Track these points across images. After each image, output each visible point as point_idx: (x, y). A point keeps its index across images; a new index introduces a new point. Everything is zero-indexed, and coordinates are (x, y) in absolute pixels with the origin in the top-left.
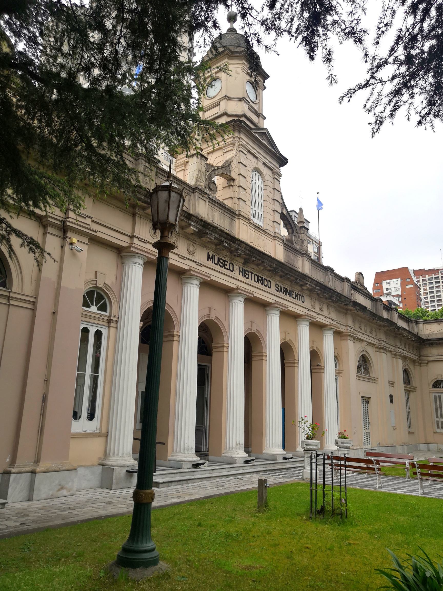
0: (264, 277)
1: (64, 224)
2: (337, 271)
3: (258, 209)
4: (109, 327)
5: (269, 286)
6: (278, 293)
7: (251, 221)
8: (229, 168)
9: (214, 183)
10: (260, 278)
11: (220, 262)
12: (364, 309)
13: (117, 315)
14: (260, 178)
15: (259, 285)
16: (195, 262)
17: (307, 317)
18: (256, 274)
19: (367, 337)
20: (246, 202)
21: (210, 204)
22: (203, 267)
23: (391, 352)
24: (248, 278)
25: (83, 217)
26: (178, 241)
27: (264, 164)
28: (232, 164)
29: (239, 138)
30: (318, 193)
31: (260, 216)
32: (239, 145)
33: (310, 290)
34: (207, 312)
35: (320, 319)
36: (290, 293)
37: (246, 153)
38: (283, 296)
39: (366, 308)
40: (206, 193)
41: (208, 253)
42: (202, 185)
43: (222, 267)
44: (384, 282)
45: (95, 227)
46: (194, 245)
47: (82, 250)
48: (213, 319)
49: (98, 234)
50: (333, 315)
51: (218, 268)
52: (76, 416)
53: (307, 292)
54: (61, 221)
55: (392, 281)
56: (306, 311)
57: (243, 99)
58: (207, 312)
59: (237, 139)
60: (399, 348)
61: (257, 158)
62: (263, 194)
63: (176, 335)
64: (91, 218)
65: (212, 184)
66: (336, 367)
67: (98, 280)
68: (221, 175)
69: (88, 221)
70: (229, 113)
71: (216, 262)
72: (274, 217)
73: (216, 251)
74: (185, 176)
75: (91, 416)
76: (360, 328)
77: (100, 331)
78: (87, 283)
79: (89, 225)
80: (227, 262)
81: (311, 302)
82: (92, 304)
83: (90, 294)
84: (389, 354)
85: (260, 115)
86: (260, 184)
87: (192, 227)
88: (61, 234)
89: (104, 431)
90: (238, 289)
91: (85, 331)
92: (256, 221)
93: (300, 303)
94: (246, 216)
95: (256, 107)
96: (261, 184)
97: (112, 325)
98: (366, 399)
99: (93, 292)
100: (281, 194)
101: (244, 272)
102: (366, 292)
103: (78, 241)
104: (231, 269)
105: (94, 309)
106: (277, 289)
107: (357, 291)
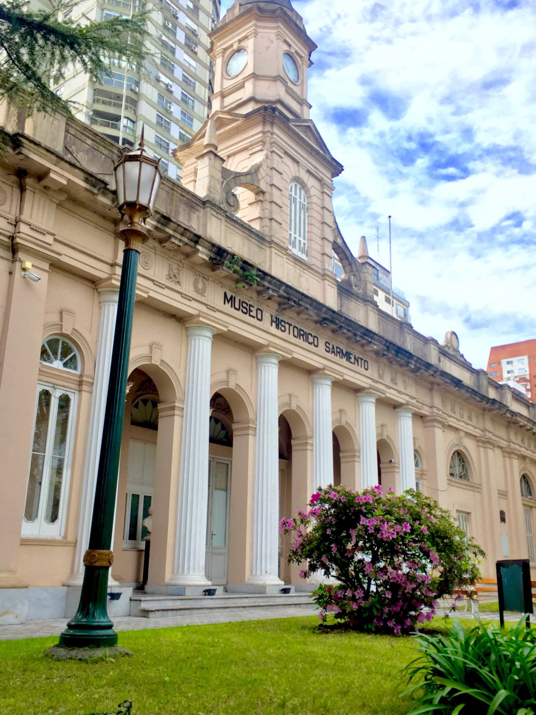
1: (12, 241)
2: (415, 328)
3: (296, 232)
4: (80, 391)
5: (316, 344)
7: (288, 252)
8: (257, 175)
9: (234, 195)
10: (302, 333)
11: (243, 307)
12: (458, 383)
13: (91, 373)
14: (303, 192)
15: (300, 342)
16: (206, 305)
17: (371, 391)
18: (297, 325)
19: (463, 424)
20: (281, 224)
21: (228, 225)
23: (501, 448)
24: (284, 331)
25: (41, 232)
26: (181, 273)
28: (261, 170)
30: (390, 217)
31: (302, 245)
32: (271, 144)
33: (377, 353)
34: (223, 376)
35: (392, 395)
36: (348, 356)
37: (282, 155)
38: (337, 359)
39: (460, 381)
40: (221, 209)
41: (225, 293)
42: (218, 197)
43: (246, 313)
44: (504, 362)
45: (58, 247)
46: (204, 280)
47: (39, 279)
48: (233, 388)
49: (63, 259)
50: (412, 390)
51: (239, 314)
52: (30, 514)
53: (373, 356)
54: (9, 237)
55: (515, 360)
56: (370, 382)
57: (277, 78)
58: (223, 376)
59: (269, 135)
60: (514, 443)
61: (297, 162)
62: (307, 214)
63: (178, 407)
64: (53, 235)
65: (232, 197)
66: (417, 465)
67: (63, 323)
68: (245, 185)
69: (49, 239)
70: (258, 97)
71: (237, 306)
72: (323, 246)
73: (237, 290)
74: (195, 187)
75: (54, 517)
76: (453, 410)
77: (67, 396)
78: (46, 327)
79: (50, 245)
80: (253, 307)
81: (379, 371)
82: (56, 358)
83: (52, 343)
84: (498, 452)
85: (303, 102)
86: (302, 201)
87: (200, 255)
88: (9, 255)
89: (70, 538)
91: (45, 396)
92: (296, 252)
93: (362, 370)
94: (282, 244)
95: (296, 89)
96: (305, 201)
97: (84, 387)
98: (464, 515)
99: (57, 341)
100: (334, 215)
101: (278, 323)
102: (462, 359)
103: (33, 266)
104: (259, 317)
105: (58, 364)
106: (328, 349)
107: (449, 358)
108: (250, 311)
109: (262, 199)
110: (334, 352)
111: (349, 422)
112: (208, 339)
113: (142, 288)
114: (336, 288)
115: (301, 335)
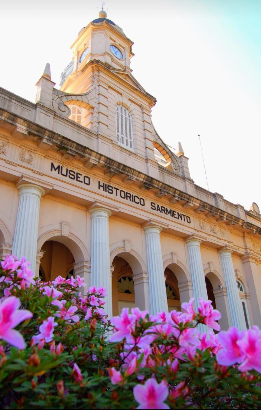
0: (134, 195)
6: (156, 211)
10: (128, 195)
15: (128, 201)
16: (32, 170)
22: (44, 176)
24: (112, 193)
27: (130, 100)
29: (99, 76)
30: (199, 135)
36: (172, 213)
37: (107, 88)
38: (163, 214)
43: (74, 179)
59: (97, 77)
61: (121, 94)
71: (64, 173)
81: (200, 223)
90: (193, 235)
106: (154, 208)
108: (77, 177)
109: (92, 112)
110: (159, 210)
111: (216, 269)
112: (37, 197)
113: (26, 176)
114: (158, 168)
115: (127, 196)
